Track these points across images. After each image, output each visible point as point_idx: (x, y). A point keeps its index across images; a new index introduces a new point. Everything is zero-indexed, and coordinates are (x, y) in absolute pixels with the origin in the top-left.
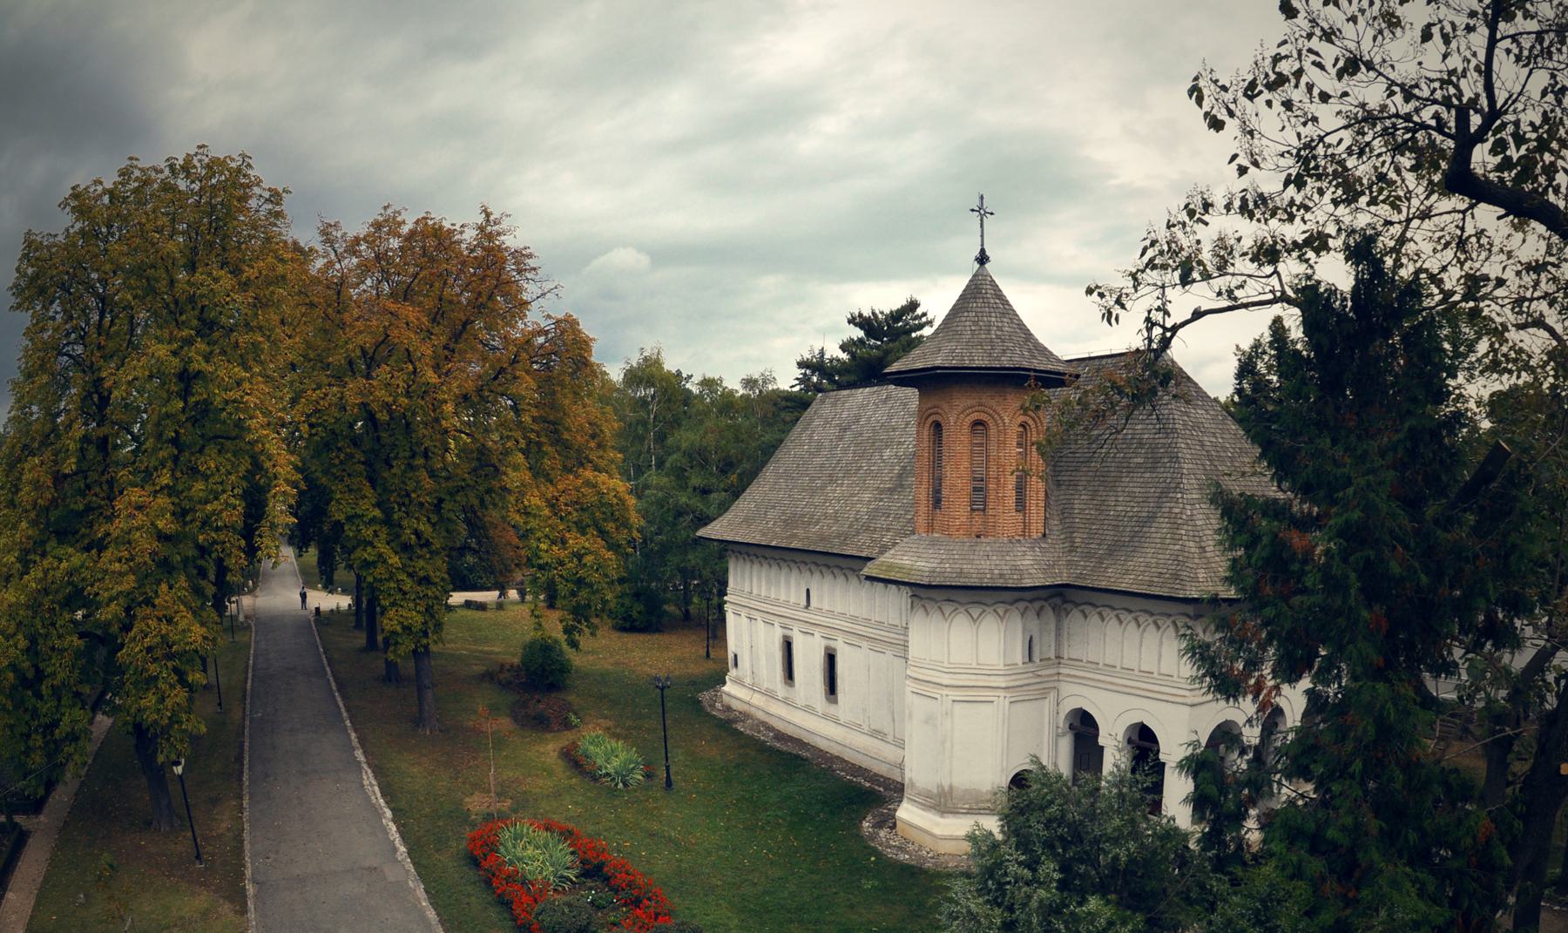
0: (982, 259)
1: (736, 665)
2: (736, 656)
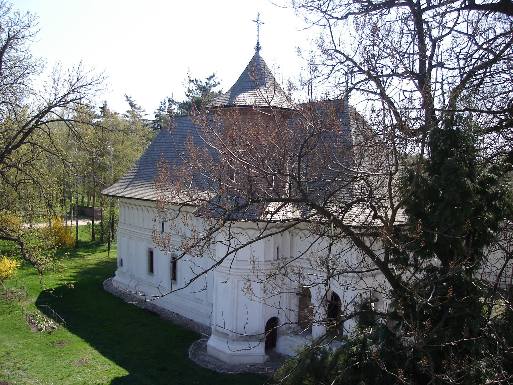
0: (258, 48)
1: (122, 265)
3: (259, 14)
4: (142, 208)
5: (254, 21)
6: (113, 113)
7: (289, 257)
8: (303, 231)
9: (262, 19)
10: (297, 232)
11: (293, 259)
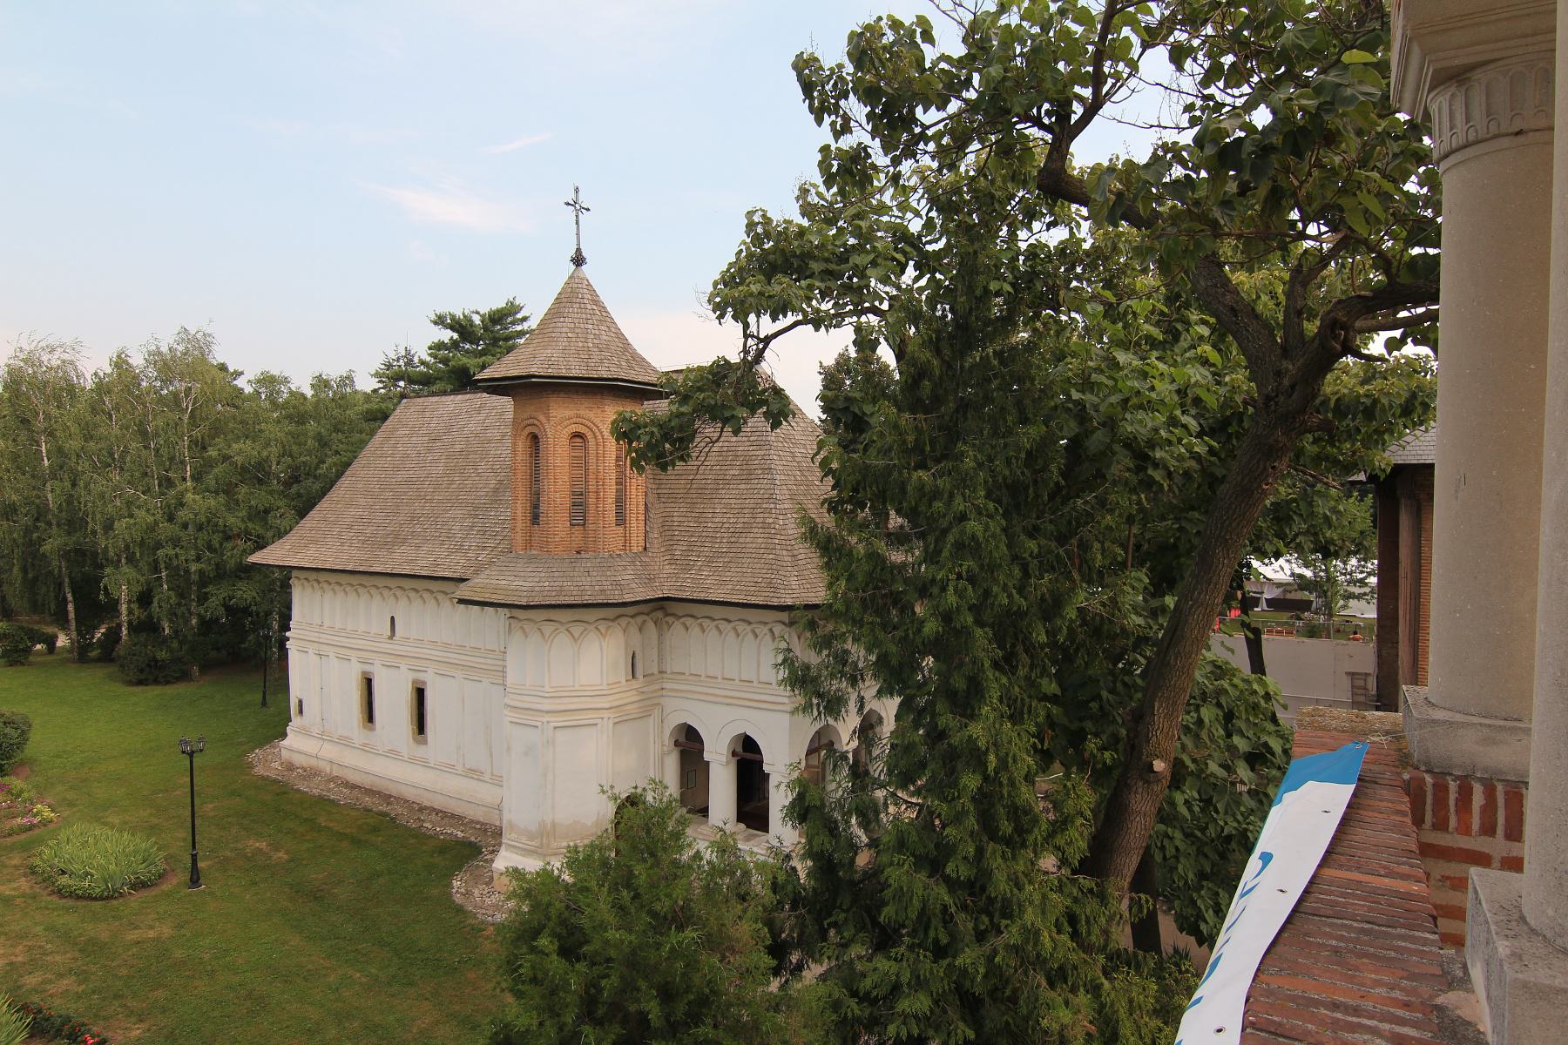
0: (578, 260)
1: (301, 712)
2: (301, 702)
3: (577, 190)
4: (771, 630)
5: (588, 210)
6: (830, 481)
7: (656, 672)
8: (682, 620)
9: (584, 200)
10: (670, 622)
11: (323, 647)
